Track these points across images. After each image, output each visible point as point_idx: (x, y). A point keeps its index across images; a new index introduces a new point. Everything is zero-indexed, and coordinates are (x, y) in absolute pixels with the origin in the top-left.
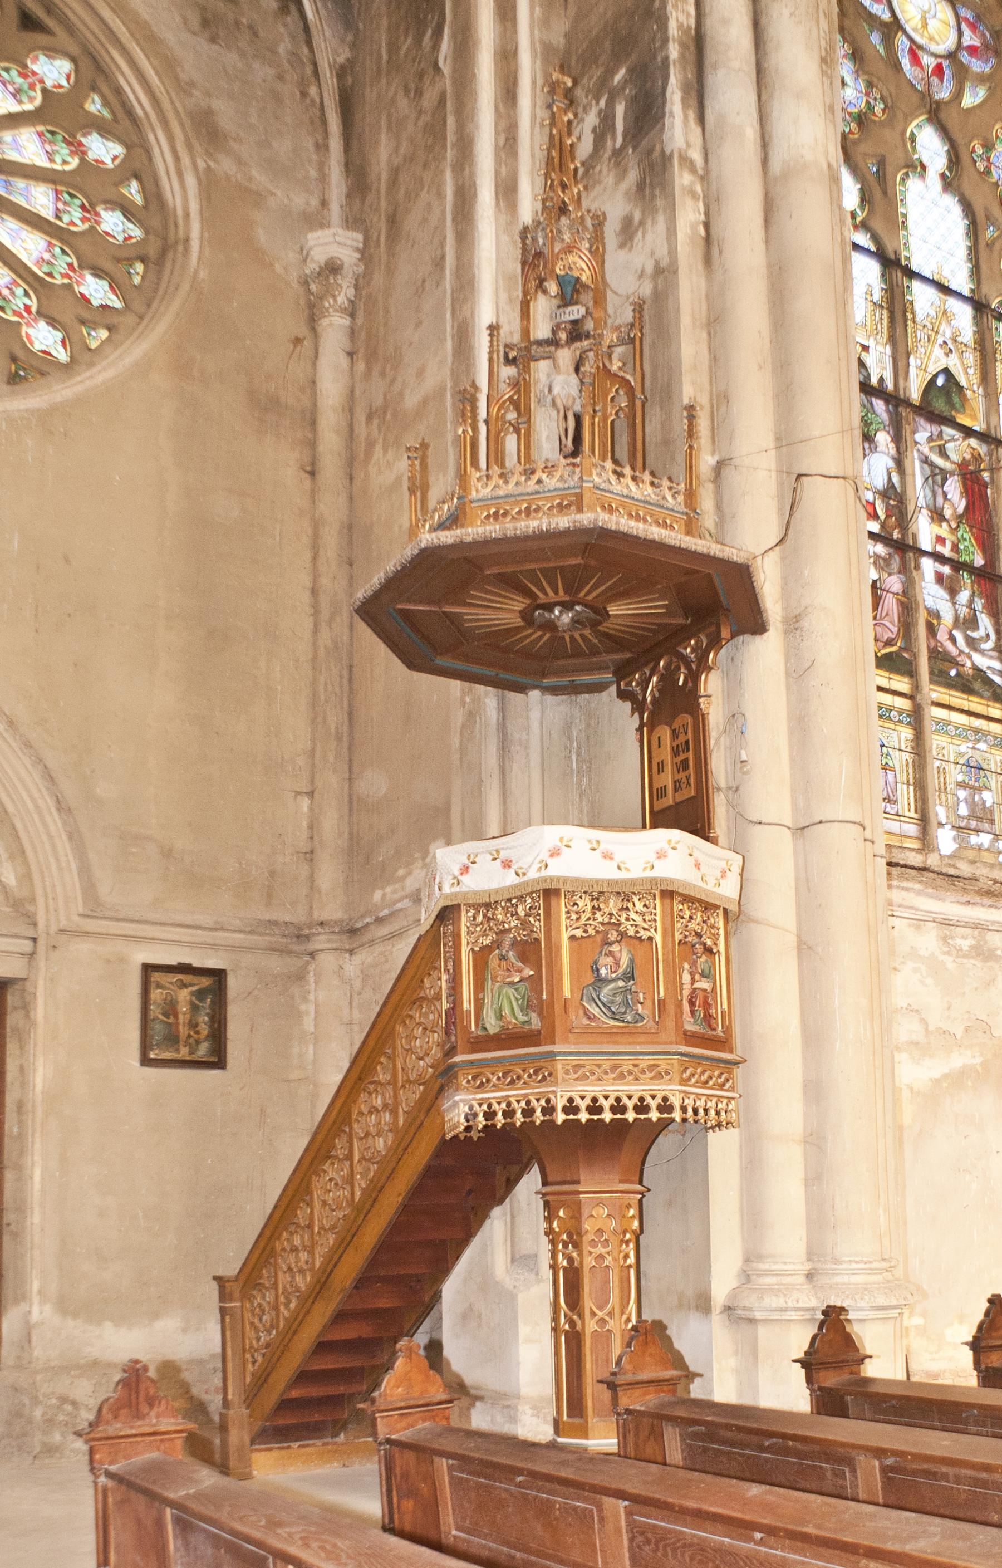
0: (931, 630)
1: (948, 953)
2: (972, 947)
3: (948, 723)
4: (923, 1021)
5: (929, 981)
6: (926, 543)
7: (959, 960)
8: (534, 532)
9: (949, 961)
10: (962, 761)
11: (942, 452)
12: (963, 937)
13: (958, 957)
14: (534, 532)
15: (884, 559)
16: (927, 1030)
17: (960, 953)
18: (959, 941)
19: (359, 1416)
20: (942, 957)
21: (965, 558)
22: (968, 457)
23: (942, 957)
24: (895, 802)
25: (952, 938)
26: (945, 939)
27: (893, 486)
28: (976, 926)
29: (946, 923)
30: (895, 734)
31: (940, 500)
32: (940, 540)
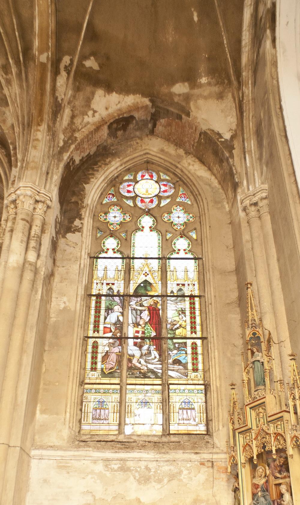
0: (130, 361)
1: (108, 471)
2: (119, 468)
3: (135, 389)
4: (94, 496)
5: (98, 481)
6: (131, 335)
7: (112, 473)
8: (93, 169)
9: (108, 474)
10: (139, 401)
11: (141, 305)
12: (115, 464)
13: (112, 471)
14: (93, 169)
15: (112, 343)
16: (95, 499)
17: (112, 470)
18: (113, 466)
19: (17, 263)
20: (104, 472)
21: (147, 335)
22: (152, 303)
23: (104, 472)
24: (107, 420)
25: (109, 465)
26: (106, 466)
27: (119, 321)
28: (121, 460)
29: (108, 460)
30: (110, 398)
31: (138, 319)
32: (137, 332)
